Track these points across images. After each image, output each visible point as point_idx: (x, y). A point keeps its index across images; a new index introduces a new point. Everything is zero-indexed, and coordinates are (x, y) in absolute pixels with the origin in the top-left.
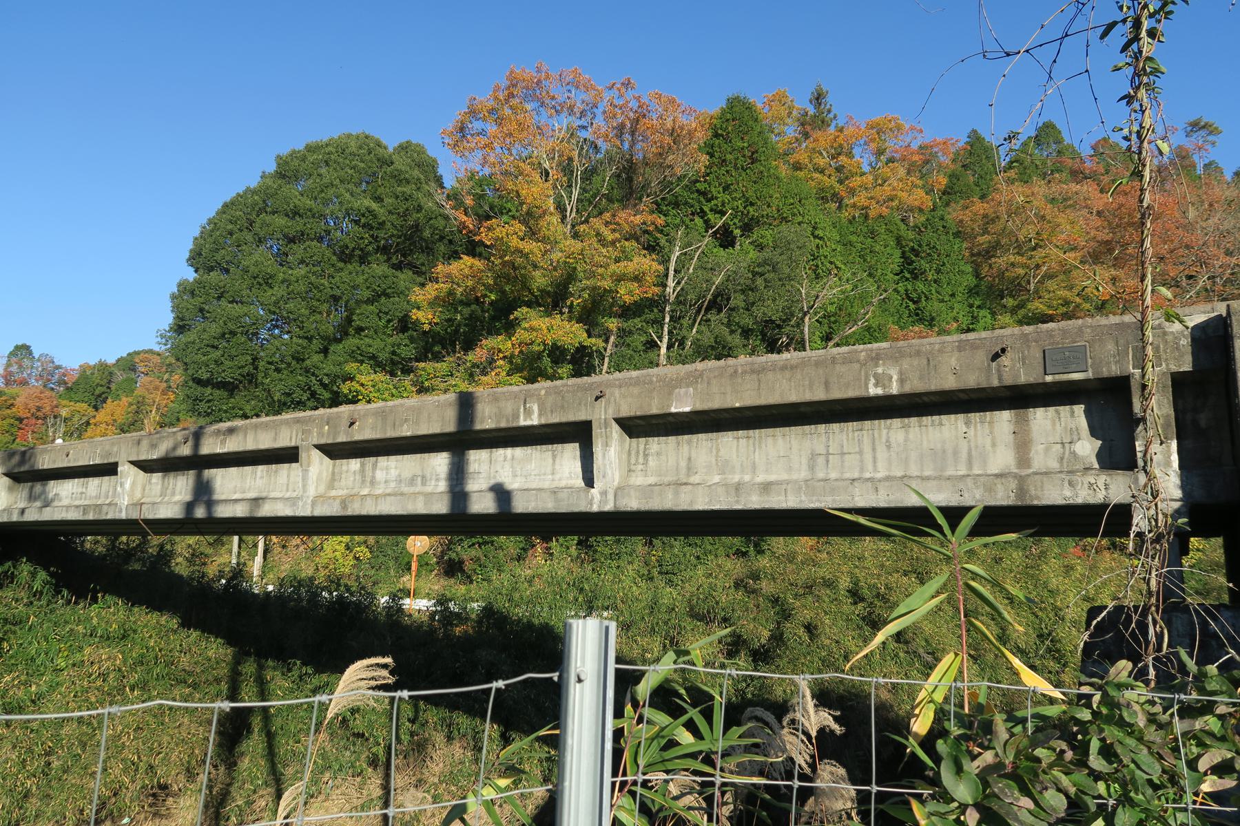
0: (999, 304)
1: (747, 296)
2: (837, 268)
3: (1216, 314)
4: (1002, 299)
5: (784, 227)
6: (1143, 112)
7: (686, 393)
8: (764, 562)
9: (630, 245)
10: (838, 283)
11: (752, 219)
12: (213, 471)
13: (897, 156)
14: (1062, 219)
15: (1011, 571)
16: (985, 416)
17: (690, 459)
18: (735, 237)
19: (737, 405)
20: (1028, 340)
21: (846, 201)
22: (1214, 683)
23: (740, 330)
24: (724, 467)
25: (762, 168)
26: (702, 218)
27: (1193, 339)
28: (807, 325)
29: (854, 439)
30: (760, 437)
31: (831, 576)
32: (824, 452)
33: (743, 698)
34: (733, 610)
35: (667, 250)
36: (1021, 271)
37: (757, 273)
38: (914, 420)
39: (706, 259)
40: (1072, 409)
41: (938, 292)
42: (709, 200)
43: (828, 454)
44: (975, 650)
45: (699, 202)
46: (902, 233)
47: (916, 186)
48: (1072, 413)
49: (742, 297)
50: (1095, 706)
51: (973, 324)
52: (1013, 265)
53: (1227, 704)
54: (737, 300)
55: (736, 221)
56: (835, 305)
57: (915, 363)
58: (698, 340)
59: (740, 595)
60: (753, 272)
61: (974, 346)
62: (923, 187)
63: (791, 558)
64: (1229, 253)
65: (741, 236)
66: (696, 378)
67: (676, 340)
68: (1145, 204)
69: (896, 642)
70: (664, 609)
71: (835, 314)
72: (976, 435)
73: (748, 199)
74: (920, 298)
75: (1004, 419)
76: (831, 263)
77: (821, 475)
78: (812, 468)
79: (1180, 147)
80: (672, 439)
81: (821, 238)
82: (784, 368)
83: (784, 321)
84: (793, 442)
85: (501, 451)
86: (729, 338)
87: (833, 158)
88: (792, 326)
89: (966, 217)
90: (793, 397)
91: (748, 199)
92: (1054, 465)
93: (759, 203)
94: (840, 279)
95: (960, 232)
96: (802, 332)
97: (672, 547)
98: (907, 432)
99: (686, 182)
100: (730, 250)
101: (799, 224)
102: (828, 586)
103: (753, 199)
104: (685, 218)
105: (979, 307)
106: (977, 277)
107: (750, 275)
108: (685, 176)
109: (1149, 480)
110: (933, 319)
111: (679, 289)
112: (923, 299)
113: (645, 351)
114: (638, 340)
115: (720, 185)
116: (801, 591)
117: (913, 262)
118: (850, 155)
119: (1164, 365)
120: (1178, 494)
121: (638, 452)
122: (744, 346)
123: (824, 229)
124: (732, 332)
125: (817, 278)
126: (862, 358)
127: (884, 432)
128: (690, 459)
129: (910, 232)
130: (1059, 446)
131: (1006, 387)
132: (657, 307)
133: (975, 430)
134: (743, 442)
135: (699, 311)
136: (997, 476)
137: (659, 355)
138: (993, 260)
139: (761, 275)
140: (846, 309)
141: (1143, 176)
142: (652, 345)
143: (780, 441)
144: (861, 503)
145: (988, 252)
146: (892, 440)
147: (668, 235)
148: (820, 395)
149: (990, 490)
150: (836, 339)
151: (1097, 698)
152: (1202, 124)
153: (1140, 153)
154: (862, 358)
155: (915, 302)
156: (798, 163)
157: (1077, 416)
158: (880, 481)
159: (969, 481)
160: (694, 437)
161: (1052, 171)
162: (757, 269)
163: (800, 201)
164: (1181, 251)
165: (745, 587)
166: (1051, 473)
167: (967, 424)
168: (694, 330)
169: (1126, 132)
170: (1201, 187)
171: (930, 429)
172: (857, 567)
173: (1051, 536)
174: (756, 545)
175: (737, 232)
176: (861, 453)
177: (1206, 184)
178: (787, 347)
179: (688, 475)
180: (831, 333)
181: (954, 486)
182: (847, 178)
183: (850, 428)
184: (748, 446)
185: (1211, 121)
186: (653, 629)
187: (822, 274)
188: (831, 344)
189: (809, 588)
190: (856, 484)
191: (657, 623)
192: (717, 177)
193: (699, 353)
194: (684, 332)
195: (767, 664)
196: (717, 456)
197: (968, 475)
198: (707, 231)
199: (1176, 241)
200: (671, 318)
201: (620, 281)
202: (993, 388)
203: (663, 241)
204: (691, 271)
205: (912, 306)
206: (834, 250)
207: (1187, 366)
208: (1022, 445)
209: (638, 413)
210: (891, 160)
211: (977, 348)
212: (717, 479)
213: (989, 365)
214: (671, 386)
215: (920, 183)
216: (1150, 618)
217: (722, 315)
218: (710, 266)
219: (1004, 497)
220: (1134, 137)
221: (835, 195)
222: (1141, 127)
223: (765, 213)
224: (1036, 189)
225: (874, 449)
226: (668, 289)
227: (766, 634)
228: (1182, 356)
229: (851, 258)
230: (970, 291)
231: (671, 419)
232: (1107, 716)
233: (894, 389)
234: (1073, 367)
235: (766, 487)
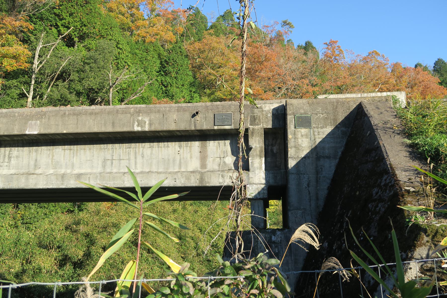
0: (203, 92)
1: (80, 74)
2: (128, 65)
3: (282, 104)
4: (204, 89)
5: (102, 40)
6: (245, 7)
7: (35, 124)
8: (82, 215)
9: (12, 38)
10: (128, 73)
11: (85, 34)
12: (289, 166)
13: (161, 13)
14: (231, 56)
15: (201, 217)
16: (188, 143)
17: (36, 160)
18: (75, 42)
19: (65, 132)
20: (208, 109)
21: (135, 32)
22: (228, 269)
23: (75, 92)
24: (56, 165)
25: (91, 7)
26: (56, 29)
27: (273, 114)
28: (111, 93)
29: (126, 152)
30: (77, 150)
31: (117, 222)
32: (111, 158)
33: (67, 288)
34: (63, 242)
35: (35, 44)
36: (213, 78)
37: (86, 63)
38: (155, 144)
39: (58, 52)
40: (225, 142)
41: (176, 83)
42: (61, 20)
43: (113, 159)
44: (184, 254)
45: (55, 19)
46: (161, 52)
47: (169, 30)
48: (225, 144)
49: (77, 74)
50: (172, 287)
51: (191, 100)
52: (210, 74)
53: (232, 279)
54: (74, 76)
55: (76, 33)
56: (126, 84)
57: (157, 116)
58: (51, 95)
59: (68, 233)
60: (84, 62)
61: (184, 110)
62: (172, 31)
63: (98, 213)
64: (294, 80)
65: (78, 42)
66: (41, 116)
67: (38, 94)
68: (244, 50)
69: (148, 253)
70: (23, 243)
71: (126, 89)
72: (183, 153)
73: (83, 22)
74: (168, 85)
75: (196, 144)
76: (125, 62)
77: (108, 170)
78: (104, 166)
79: (279, 31)
80: (26, 149)
81: (121, 49)
82: (91, 114)
83: (99, 90)
84: (95, 153)
86: (69, 96)
87: (129, 9)
88: (103, 93)
89: (191, 48)
90: (96, 129)
91: (83, 22)
92: (216, 167)
93: (89, 26)
94: (129, 71)
95: (188, 55)
96: (109, 96)
97: (30, 208)
98: (152, 150)
99: (48, 7)
100: (72, 48)
101: (110, 40)
102: (115, 227)
103: (86, 23)
104: (46, 27)
105: (194, 92)
106: (194, 78)
107: (82, 64)
108: (47, 4)
109: (240, 175)
110: (173, 96)
111: (41, 66)
112: (169, 86)
113: (19, 99)
114: (15, 92)
115: (67, 12)
116: (101, 230)
117: (166, 67)
118: (138, 9)
119: (261, 125)
120: (264, 181)
121: (5, 156)
122: (77, 101)
123: (122, 44)
124: (71, 93)
125: (118, 69)
126: (132, 112)
127: (141, 149)
128: (36, 160)
129: (165, 52)
130: (219, 159)
131: (197, 130)
132: (27, 74)
133: (183, 150)
134: (67, 152)
135: (52, 80)
136: (191, 172)
137: (27, 102)
138: (202, 71)
139: (88, 64)
140: (132, 87)
141: (243, 36)
142: (23, 96)
143: (88, 152)
144: (116, 187)
145: (199, 67)
146: (145, 153)
147: (35, 35)
148: (109, 129)
149: (188, 179)
150: (126, 101)
151: (174, 282)
152: (288, 23)
153: (243, 26)
154: (132, 112)
155: (165, 87)
156: (111, 8)
158: (137, 174)
159: (179, 174)
160: (40, 148)
161: (229, 33)
162: (86, 61)
163: (111, 28)
164: (277, 76)
165: (71, 229)
166: (215, 171)
167: (180, 147)
168: (49, 90)
169: (238, 14)
170: (285, 50)
171: (163, 148)
172: (130, 217)
174: (79, 207)
175: (76, 39)
176: (129, 159)
177: (287, 48)
178: (100, 103)
179: (35, 169)
180: (123, 98)
181: (172, 177)
182: (136, 20)
183: (124, 147)
184: (70, 154)
185: (291, 22)
186: (16, 255)
187: (120, 67)
188: (123, 103)
189: (105, 228)
190: (126, 175)
191: (19, 252)
192: (66, 8)
193: (51, 102)
194: (43, 90)
195: (81, 269)
196: (52, 159)
197: (179, 172)
198: (59, 36)
199: (275, 72)
200: (36, 81)
201: (4, 58)
202: (192, 131)
203: (32, 38)
204: (48, 57)
205: (164, 89)
206: (127, 56)
207: (270, 126)
208: (203, 158)
209: (6, 133)
210: (158, 15)
211: (186, 111)
212: (51, 171)
213: (191, 119)
214: (27, 118)
215: (171, 29)
216: (237, 237)
217: (65, 83)
218: (60, 55)
219: (194, 182)
220: (241, 18)
221: (129, 28)
222: (244, 14)
223: (92, 31)
224: (221, 40)
225: (136, 158)
226: (34, 65)
227: (81, 253)
229: (135, 61)
230: (191, 84)
231: (26, 137)
232: (177, 290)
233: (147, 129)
234: (226, 123)
235: (79, 176)
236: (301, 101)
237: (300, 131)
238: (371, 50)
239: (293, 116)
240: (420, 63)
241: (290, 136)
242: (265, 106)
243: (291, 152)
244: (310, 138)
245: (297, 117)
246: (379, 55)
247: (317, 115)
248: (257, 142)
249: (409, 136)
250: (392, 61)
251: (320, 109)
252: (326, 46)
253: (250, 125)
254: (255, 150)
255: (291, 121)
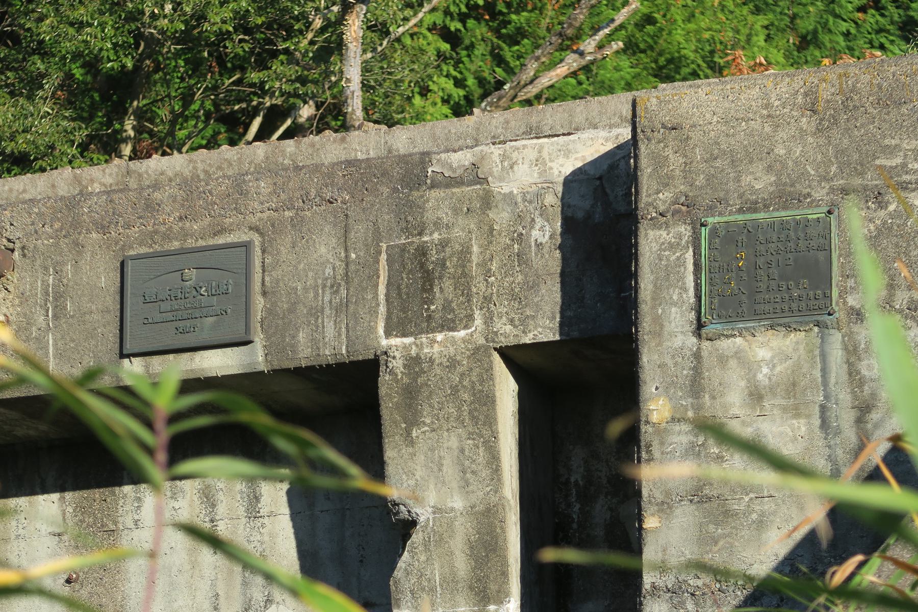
20: (76, 225)
27: (570, 224)
35: (678, 77)
119: (478, 321)
131: (298, 372)
173: (369, 360)
228: (532, 287)
234: (206, 328)
236: (755, 92)
237: (738, 355)
239: (685, 231)
242: (504, 157)
244: (823, 409)
245: (714, 233)
247: (882, 205)
248: (450, 470)
253: (388, 334)
254: (439, 540)
255: (670, 274)
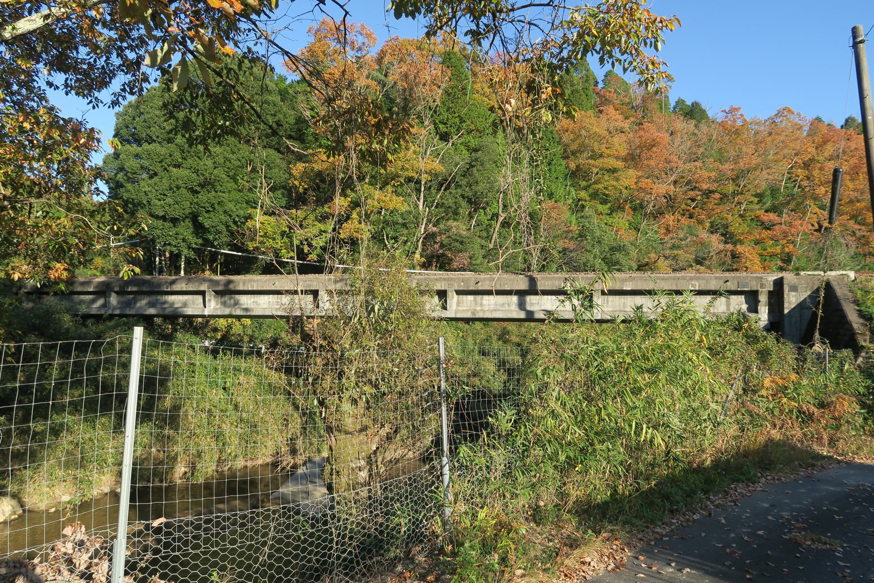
85: (546, 296)
157: (742, 298)
214: (624, 281)
238: (783, 107)
240: (853, 116)
241: (785, 296)
243: (786, 305)
246: (793, 113)
249: (858, 305)
250: (810, 116)
251: (803, 282)
252: (724, 114)
